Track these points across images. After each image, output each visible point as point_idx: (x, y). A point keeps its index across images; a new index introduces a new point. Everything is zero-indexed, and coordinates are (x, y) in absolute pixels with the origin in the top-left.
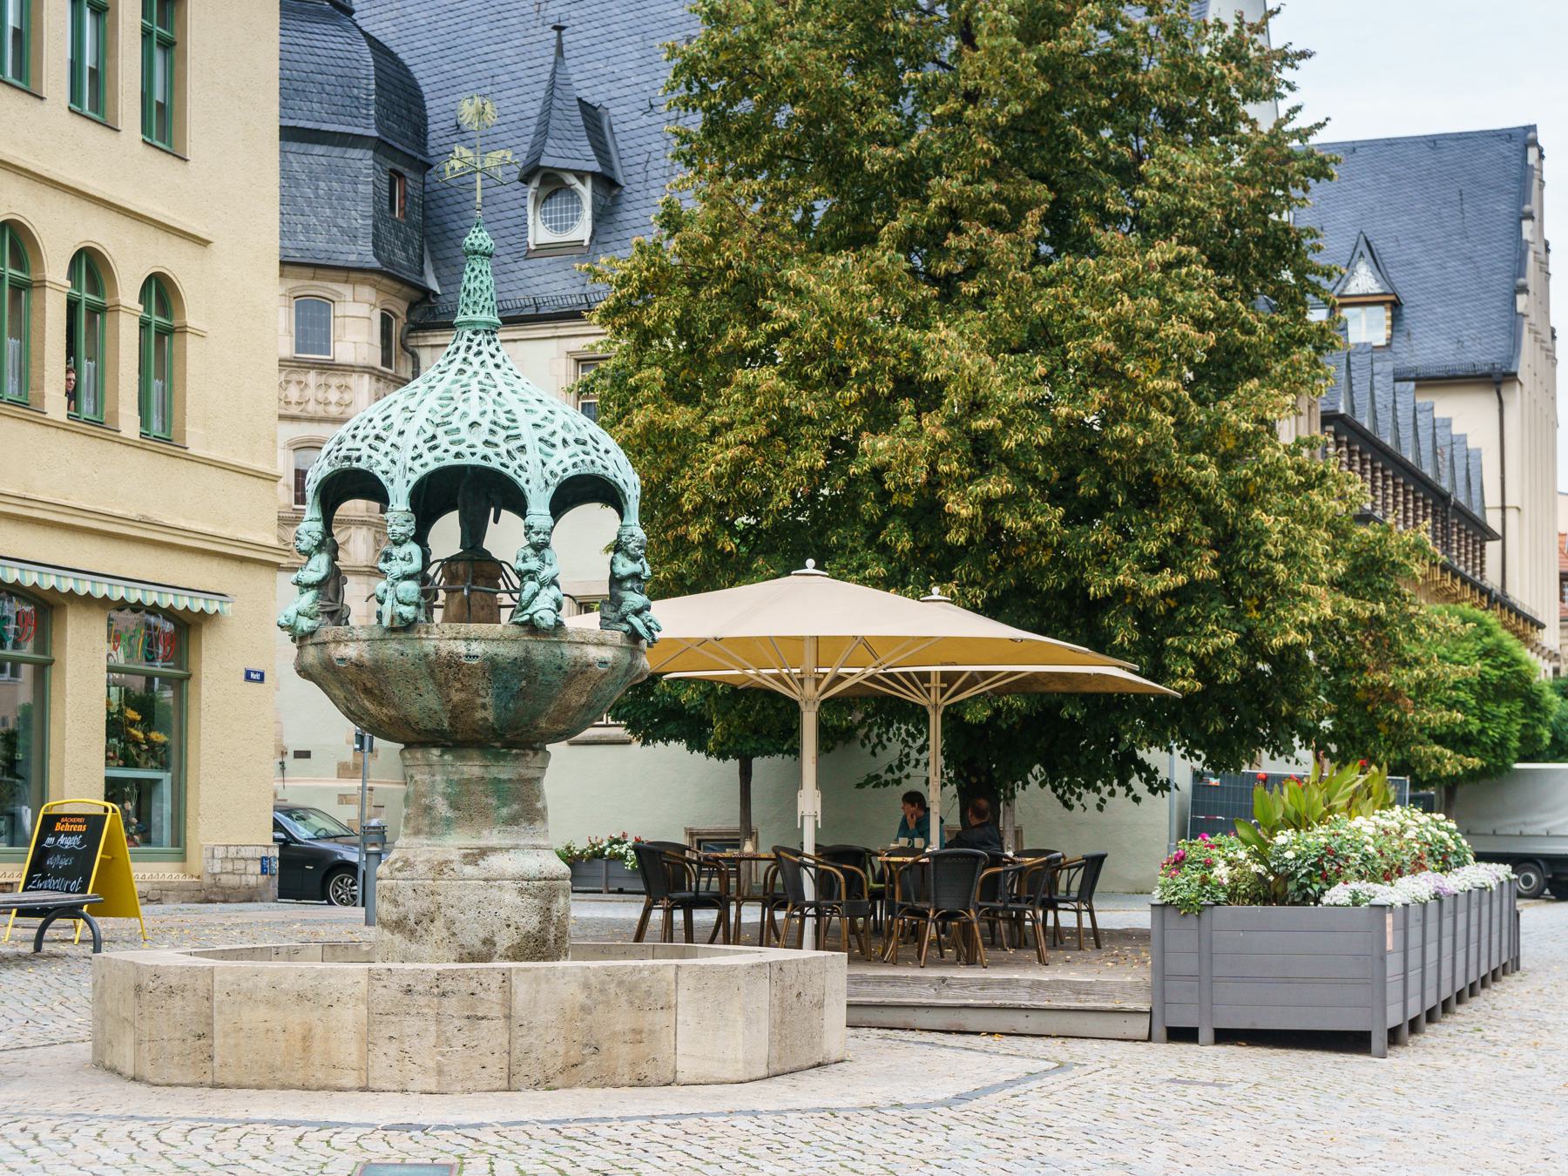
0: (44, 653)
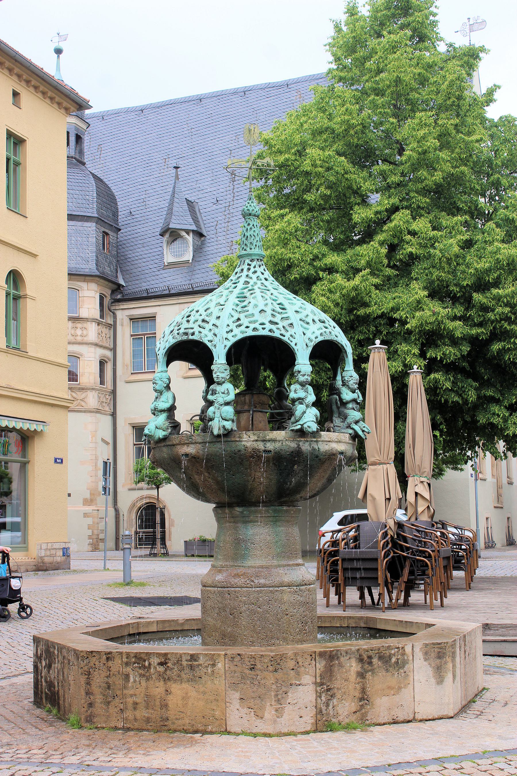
0: (25, 458)
